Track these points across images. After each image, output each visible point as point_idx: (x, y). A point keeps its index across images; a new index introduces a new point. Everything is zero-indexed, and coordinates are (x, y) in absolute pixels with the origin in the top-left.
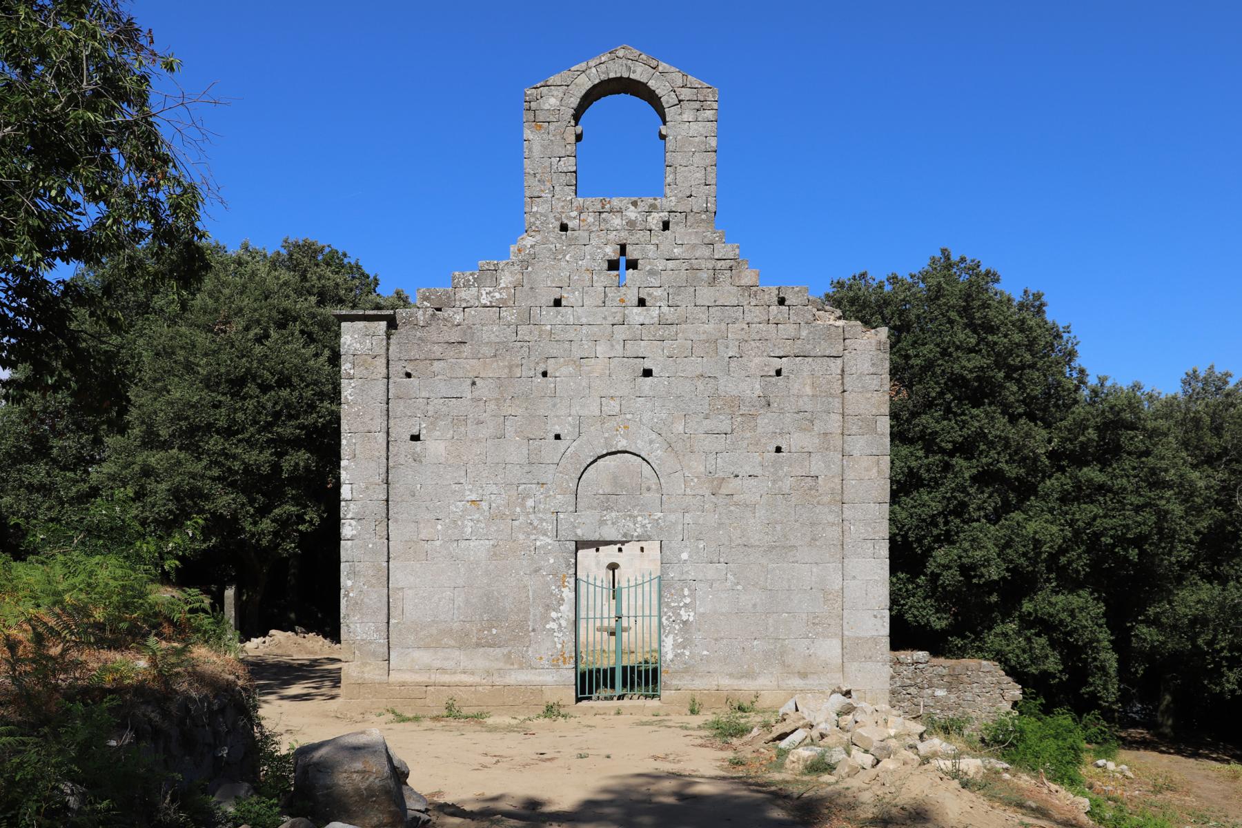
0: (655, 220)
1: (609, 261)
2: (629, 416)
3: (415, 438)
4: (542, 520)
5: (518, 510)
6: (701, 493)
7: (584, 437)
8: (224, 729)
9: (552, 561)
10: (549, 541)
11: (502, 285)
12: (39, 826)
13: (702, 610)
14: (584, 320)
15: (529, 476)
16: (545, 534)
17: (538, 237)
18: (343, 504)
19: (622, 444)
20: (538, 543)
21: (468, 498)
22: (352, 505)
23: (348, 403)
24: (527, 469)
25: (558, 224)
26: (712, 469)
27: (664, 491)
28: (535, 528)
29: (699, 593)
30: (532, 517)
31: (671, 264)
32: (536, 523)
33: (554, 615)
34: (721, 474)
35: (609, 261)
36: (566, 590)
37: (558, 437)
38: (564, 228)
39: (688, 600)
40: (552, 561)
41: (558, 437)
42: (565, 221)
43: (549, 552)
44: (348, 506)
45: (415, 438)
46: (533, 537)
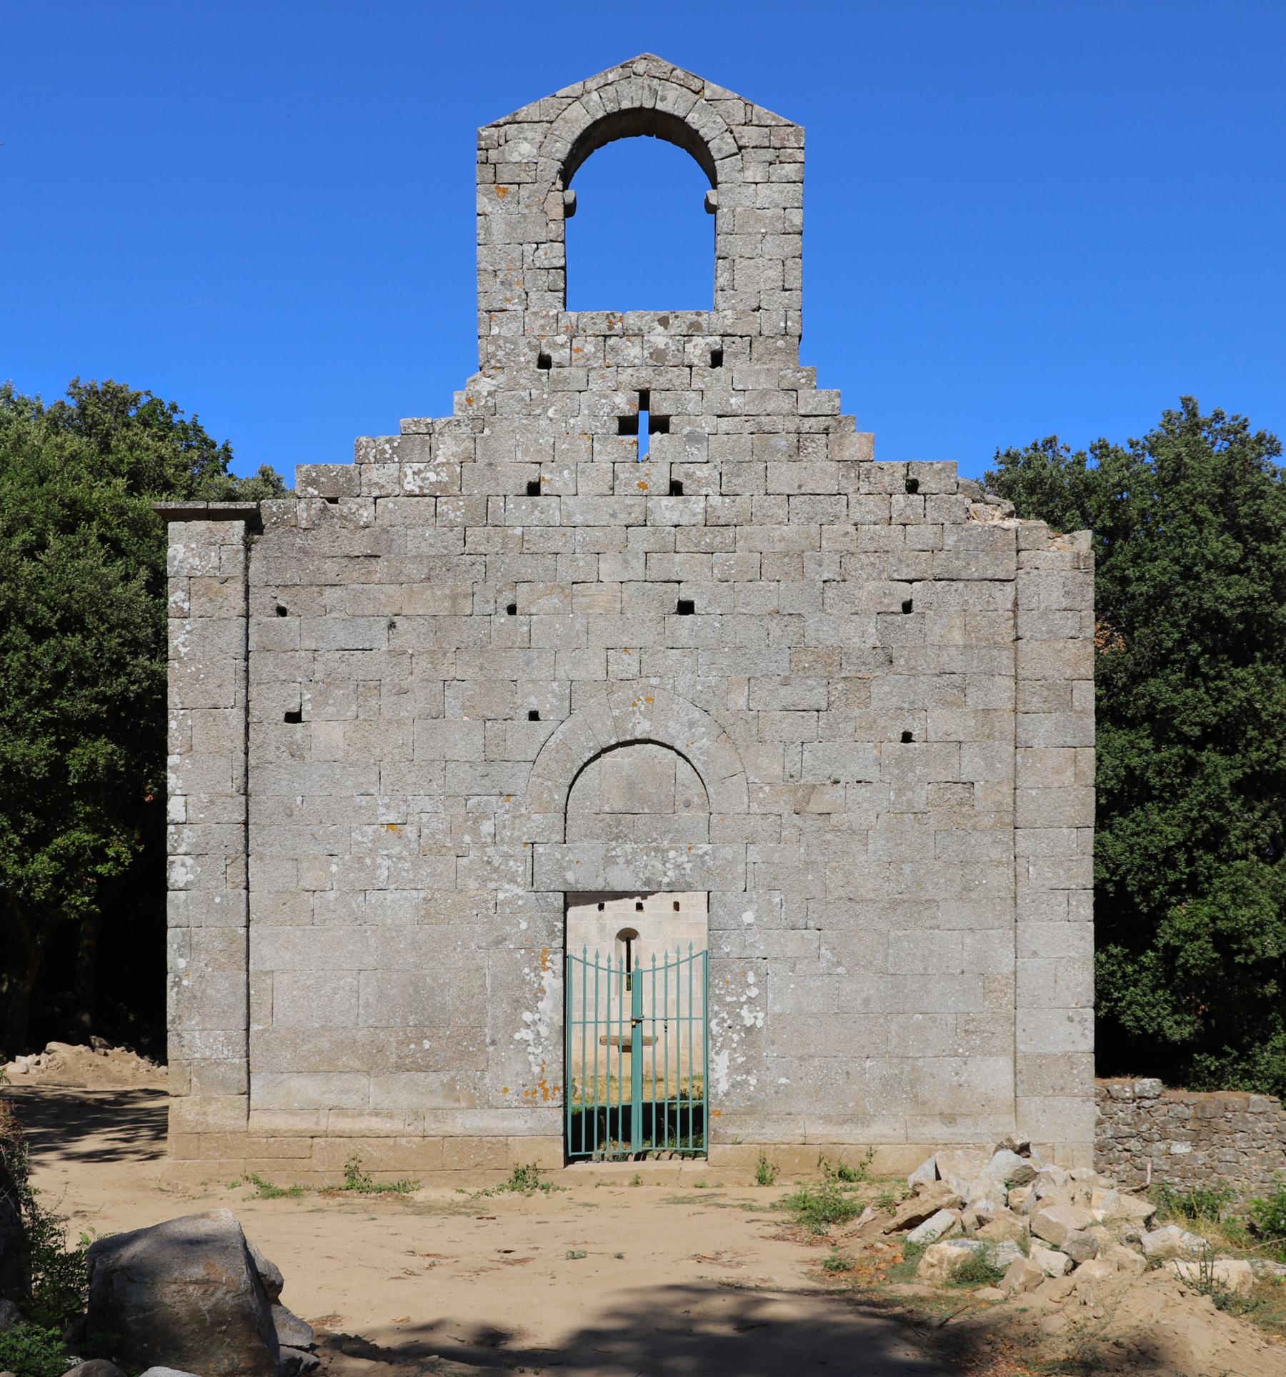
0: (698, 349)
2: (654, 681)
3: (293, 718)
4: (507, 857)
5: (467, 839)
6: (776, 810)
7: (578, 717)
9: (524, 925)
10: (520, 891)
11: (440, 459)
14: (578, 519)
16: (513, 880)
17: (501, 378)
18: (171, 828)
19: (642, 728)
20: (501, 896)
21: (383, 819)
22: (186, 832)
23: (179, 659)
24: (481, 769)
25: (534, 356)
28: (496, 870)
29: (773, 980)
30: (490, 851)
31: (725, 424)
34: (809, 779)
36: (547, 975)
37: (534, 716)
38: (544, 362)
39: (754, 992)
40: (524, 925)
41: (534, 716)
42: (547, 351)
43: (520, 910)
44: (179, 833)
45: (293, 718)
46: (492, 885)
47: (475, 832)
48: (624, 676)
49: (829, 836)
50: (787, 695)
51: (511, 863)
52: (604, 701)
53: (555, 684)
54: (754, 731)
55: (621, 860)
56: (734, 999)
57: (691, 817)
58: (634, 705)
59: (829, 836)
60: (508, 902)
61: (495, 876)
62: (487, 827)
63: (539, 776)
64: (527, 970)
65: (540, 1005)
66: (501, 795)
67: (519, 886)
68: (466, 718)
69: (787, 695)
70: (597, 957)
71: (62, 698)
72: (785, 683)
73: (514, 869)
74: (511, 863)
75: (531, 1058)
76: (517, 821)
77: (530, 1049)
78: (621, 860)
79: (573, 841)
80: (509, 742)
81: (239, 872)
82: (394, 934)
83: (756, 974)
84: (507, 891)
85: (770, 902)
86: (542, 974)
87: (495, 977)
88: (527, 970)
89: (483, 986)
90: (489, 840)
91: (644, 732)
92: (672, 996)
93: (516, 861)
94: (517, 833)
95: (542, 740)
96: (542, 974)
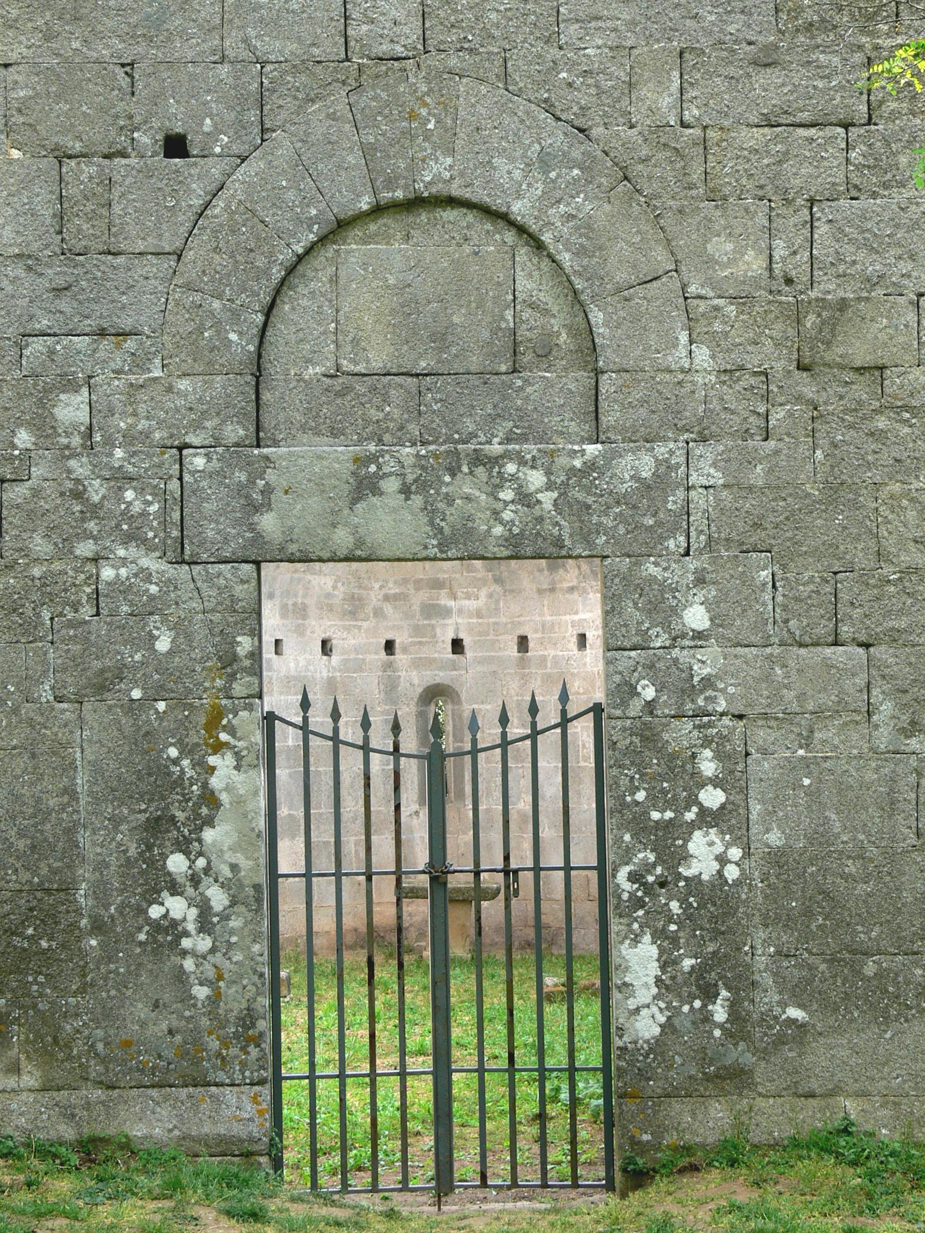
1: (400, 492)
4: (120, 479)
5: (24, 438)
6: (753, 361)
7: (283, 145)
8: (83, 576)
9: (163, 645)
10: (150, 562)
12: (924, 52)
13: (775, 838)
15: (64, 304)
16: (133, 538)
19: (436, 172)
20: (108, 573)
24: (54, 274)
26: (799, 266)
27: (607, 358)
28: (94, 511)
29: (762, 767)
30: (80, 467)
32: (97, 491)
33: (177, 863)
34: (828, 287)
35: (400, 492)
37: (175, 146)
39: (712, 798)
41: (175, 146)
43: (153, 607)
46: (85, 549)
47: (44, 426)
48: (385, 48)
49: (882, 423)
50: (769, 88)
51: (129, 495)
52: (341, 108)
53: (224, 70)
54: (696, 175)
55: (391, 485)
56: (669, 815)
57: (553, 388)
58: (413, 116)
59: (882, 423)
60: (122, 588)
61: (92, 526)
62: (72, 410)
63: (189, 287)
64: (173, 752)
65: (208, 835)
66: (102, 333)
67: (150, 549)
68: (15, 154)
69: (769, 88)
70: (336, 715)
71: (854, 864)
72: (766, 61)
73: (137, 507)
74: (129, 495)
75: (189, 964)
76: (142, 396)
77: (186, 943)
78: (391, 485)
79: (276, 444)
80: (117, 209)
81: (251, 589)
82: (507, 495)
83: (719, 756)
84: (124, 561)
85: (746, 580)
86: (212, 760)
87: (96, 768)
88: (173, 752)
89: (70, 792)
90: (76, 441)
91: (437, 178)
92: (522, 804)
93: (140, 491)
94: (143, 424)
95: (197, 202)
96: (212, 760)
